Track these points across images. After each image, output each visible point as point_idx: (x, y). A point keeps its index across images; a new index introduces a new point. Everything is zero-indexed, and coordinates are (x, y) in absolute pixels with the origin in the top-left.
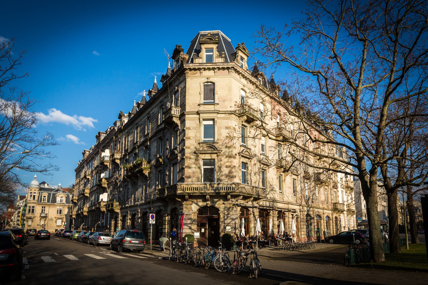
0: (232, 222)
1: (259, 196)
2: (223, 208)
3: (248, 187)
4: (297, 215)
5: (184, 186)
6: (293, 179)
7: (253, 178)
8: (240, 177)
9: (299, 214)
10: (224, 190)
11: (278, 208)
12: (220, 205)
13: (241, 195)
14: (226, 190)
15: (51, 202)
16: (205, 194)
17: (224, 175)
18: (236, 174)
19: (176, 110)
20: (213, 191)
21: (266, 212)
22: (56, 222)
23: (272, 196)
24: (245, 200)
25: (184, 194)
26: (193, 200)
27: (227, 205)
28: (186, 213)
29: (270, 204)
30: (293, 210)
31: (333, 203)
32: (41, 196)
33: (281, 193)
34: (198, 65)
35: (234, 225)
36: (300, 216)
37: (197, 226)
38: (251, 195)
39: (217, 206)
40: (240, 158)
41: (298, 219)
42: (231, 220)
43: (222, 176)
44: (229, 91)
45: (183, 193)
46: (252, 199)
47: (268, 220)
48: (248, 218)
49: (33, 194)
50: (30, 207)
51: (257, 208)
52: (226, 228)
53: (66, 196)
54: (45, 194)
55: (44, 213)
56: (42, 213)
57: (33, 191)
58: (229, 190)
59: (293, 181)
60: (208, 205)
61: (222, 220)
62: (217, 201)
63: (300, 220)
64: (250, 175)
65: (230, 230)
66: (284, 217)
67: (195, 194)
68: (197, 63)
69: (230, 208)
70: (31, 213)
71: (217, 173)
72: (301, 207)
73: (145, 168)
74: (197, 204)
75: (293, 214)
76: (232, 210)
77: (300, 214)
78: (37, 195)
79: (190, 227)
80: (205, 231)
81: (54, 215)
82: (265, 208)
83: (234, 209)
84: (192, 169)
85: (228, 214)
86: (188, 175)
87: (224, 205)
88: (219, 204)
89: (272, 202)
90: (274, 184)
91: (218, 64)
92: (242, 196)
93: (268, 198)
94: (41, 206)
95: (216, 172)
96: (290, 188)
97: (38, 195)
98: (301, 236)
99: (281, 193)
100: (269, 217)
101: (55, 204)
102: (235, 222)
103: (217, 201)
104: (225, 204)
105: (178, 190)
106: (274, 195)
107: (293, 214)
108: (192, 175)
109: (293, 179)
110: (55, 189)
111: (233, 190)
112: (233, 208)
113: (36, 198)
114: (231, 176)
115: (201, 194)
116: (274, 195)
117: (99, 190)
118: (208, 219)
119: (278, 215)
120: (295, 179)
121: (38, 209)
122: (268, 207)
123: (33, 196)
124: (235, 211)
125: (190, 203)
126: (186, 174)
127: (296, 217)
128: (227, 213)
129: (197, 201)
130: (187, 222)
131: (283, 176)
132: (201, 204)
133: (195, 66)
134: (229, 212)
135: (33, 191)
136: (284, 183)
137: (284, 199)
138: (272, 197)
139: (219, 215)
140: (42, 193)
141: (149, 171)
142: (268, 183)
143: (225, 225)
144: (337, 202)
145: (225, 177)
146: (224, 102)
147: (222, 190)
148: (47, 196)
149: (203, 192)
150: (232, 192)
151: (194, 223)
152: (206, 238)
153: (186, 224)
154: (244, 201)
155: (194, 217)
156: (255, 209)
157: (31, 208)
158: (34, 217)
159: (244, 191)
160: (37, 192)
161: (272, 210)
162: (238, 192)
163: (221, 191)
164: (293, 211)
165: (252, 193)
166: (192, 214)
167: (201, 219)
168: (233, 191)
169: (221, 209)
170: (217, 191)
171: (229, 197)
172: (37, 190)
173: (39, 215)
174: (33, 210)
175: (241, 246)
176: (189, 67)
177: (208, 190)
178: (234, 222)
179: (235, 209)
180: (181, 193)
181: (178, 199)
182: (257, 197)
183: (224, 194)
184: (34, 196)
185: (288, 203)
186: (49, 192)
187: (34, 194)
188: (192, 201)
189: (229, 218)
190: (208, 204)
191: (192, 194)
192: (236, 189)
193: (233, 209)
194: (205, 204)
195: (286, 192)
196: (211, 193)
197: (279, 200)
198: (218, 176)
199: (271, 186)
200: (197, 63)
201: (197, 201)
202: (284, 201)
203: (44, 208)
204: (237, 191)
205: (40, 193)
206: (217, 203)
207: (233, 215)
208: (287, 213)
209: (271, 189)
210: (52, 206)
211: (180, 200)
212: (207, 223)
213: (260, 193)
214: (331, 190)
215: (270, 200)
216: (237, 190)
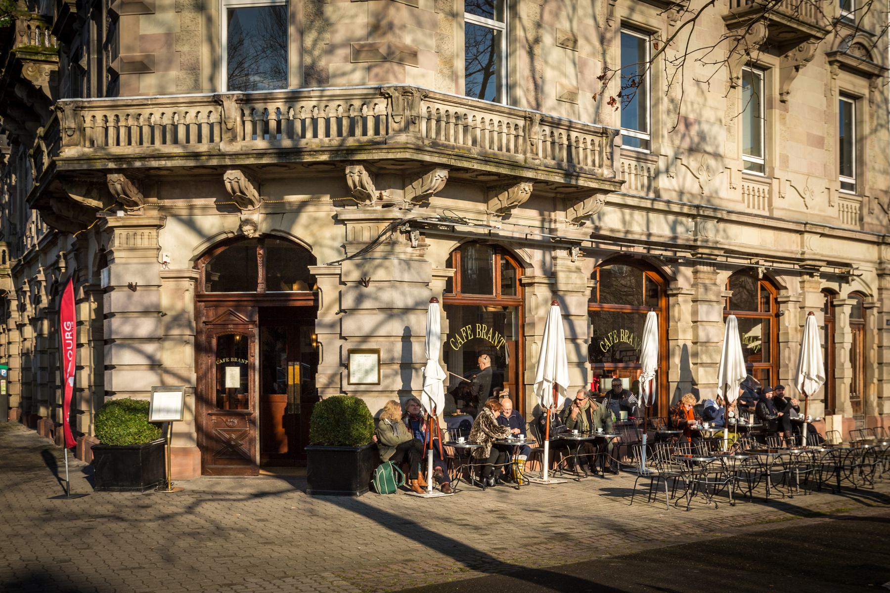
0: (383, 331)
1: (571, 172)
2: (338, 244)
3: (488, 117)
4: (856, 294)
6: (842, 93)
7: (549, 74)
8: (448, 62)
9: (875, 286)
10: (328, 134)
13: (433, 166)
14: (340, 133)
16: (214, 162)
17: (344, 45)
18: (420, 35)
20: (261, 144)
21: (654, 275)
23: (692, 186)
24: (486, 201)
25: (99, 165)
26: (167, 202)
27: (358, 226)
29: (680, 229)
30: (830, 263)
33: (760, 168)
35: (398, 347)
36: (881, 300)
37: (200, 349)
38: (514, 165)
39: (301, 232)
41: (864, 316)
42: (380, 317)
43: (331, 50)
45: (88, 159)
46: (524, 191)
48: (516, 308)
51: (576, 251)
52: (347, 366)
58: (352, 133)
59: (845, 110)
60: (248, 231)
61: (327, 314)
62: (303, 204)
63: (880, 320)
64: (531, 53)
65: (373, 378)
66: (778, 303)
67: (154, 164)
69: (375, 242)
71: (302, 33)
73: (34, 51)
74: (190, 224)
75: (834, 286)
76: (385, 258)
77: (880, 289)
79: (150, 357)
80: (244, 375)
82: (640, 249)
83: (398, 249)
84: (159, 16)
85: (363, 282)
86: (137, 55)
87: (340, 230)
88: (315, 220)
89: (693, 217)
90: (708, 114)
92: (443, 174)
93: (665, 196)
95: (292, 30)
96: (819, 142)
98: (880, 406)
99: (760, 168)
100: (672, 300)
102: (407, 330)
104: (343, 222)
105: (65, 140)
106: (703, 177)
107: (834, 286)
108: (159, 51)
109: (842, 93)
111: (377, 132)
112: (393, 244)
114: (383, 50)
115: (191, 163)
116: (703, 177)
118: (263, 312)
119: (730, 294)
120: (857, 98)
122: (665, 246)
124: (407, 263)
125: (149, 215)
126: (129, 48)
127: (854, 302)
128: (355, 275)
129: (191, 207)
130: (136, 327)
131: (776, 73)
134: (367, 267)
136: (776, 113)
137: (777, 202)
138: (696, 189)
139: (310, 282)
141: (55, 68)
142: (665, 105)
143: (348, 346)
145: (346, 59)
147: (315, 135)
149: (204, 147)
150: (374, 145)
151: (176, 332)
152: (253, 422)
153: (131, 342)
154: (482, 207)
156: (561, 254)
159: (457, 138)
161: (688, 263)
162: (405, 148)
163: (309, 141)
164: (830, 270)
165: (520, 157)
166: (163, 282)
167: (221, 311)
168: (378, 138)
170: (287, 143)
171: (357, 175)
175: (425, 469)
177: (234, 139)
178: (396, 328)
179: (405, 250)
180: (78, 159)
181: (87, 195)
182: (559, 179)
183: (324, 157)
185: (802, 229)
188: (161, 208)
189: (367, 304)
190: (247, 222)
191: (138, 164)
192: (393, 126)
193: (391, 252)
194: (231, 222)
196: (247, 155)
197: (731, 206)
198: (310, 52)
199: (688, 125)
201: (191, 207)
202: (776, 214)
204: (402, 138)
206: (304, 218)
207: (393, 284)
208: (791, 284)
209: (686, 144)
211: (94, 203)
212: (256, 331)
213: (586, 158)
215: (676, 208)
216: (400, 131)
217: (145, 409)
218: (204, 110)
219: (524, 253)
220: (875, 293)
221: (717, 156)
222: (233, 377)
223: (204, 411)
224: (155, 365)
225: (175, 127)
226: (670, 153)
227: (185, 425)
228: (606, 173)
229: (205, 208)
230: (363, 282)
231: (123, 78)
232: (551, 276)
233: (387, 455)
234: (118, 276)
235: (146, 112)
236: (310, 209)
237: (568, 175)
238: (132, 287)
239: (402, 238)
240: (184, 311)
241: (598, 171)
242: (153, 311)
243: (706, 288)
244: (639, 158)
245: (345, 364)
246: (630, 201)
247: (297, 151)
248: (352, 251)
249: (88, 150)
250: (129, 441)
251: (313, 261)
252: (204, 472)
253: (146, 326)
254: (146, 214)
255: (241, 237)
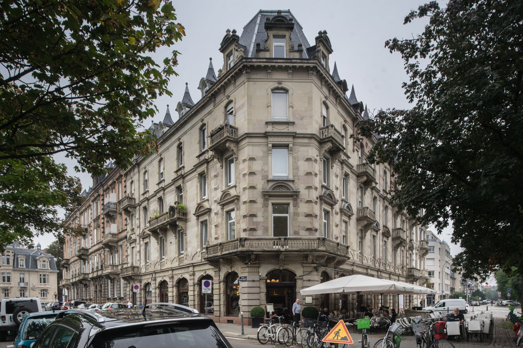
19: (232, 130)
28: (487, 281)
31: (409, 269)
34: (264, 60)
40: (321, 205)
44: (309, 103)
53: (50, 260)
55: (23, 282)
56: (21, 282)
68: (263, 59)
91: (293, 61)
117: (103, 250)
133: (260, 62)
137: (364, 262)
144: (412, 267)
146: (301, 119)
173: (17, 285)
176: (251, 64)
195: (366, 252)
200: (263, 59)
202: (364, 264)
214: (407, 251)
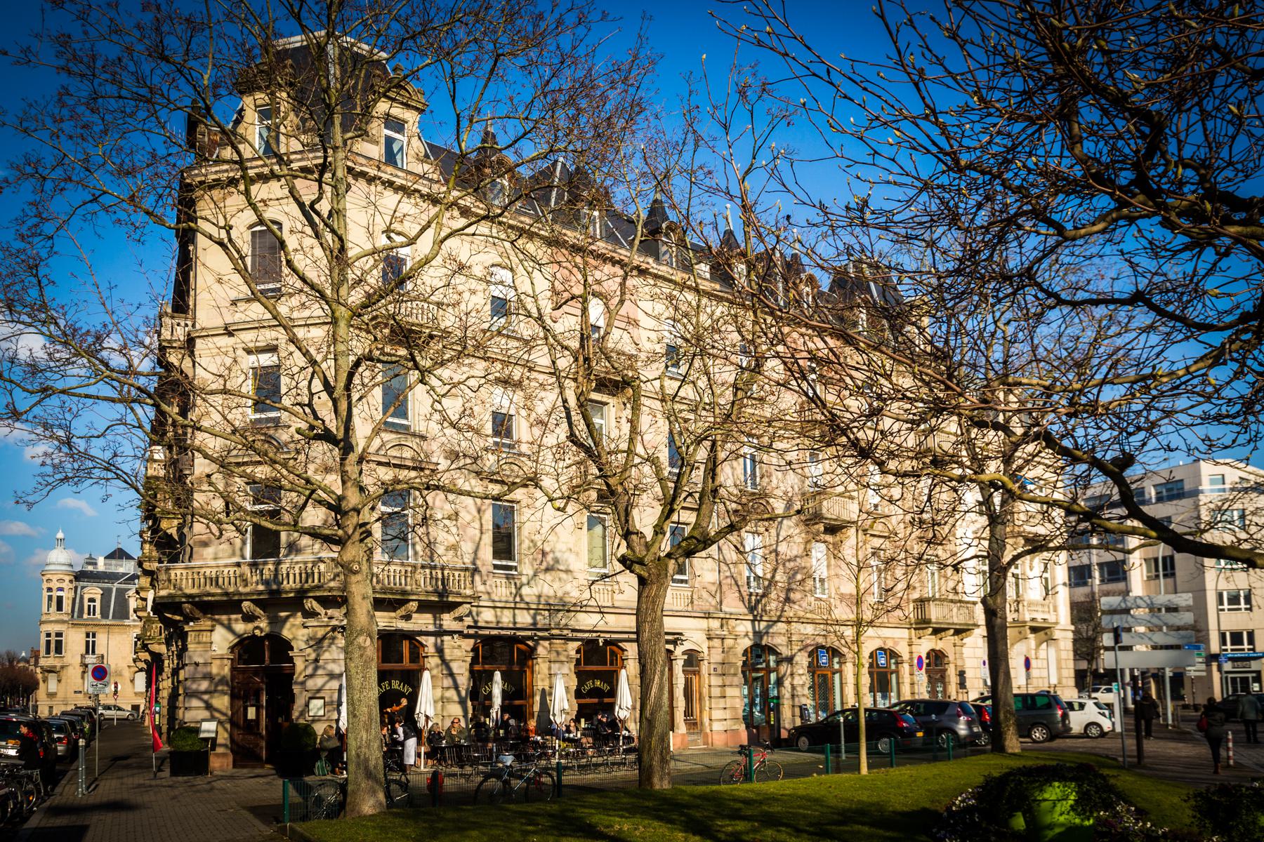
1: (443, 593)
5: (178, 572)
11: (574, 630)
12: (296, 631)
15: (114, 617)
16: (236, 598)
22: (132, 681)
23: (547, 590)
24: (394, 611)
25: (177, 600)
29: (539, 618)
31: (915, 601)
32: (82, 598)
37: (233, 697)
38: (404, 592)
39: (286, 633)
47: (532, 672)
49: (55, 594)
50: (48, 635)
54: (93, 591)
55: (93, 652)
56: (87, 652)
57: (55, 585)
58: (307, 581)
60: (257, 632)
62: (288, 617)
65: (321, 713)
69: (324, 638)
70: (52, 653)
72: (715, 624)
74: (229, 628)
78: (67, 596)
79: (206, 702)
81: (123, 658)
87: (306, 631)
90: (560, 546)
94: (83, 630)
97: (72, 594)
101: (127, 622)
103: (288, 617)
110: (125, 574)
112: (334, 638)
113: (67, 606)
121: (75, 641)
123: (55, 600)
128: (313, 656)
132: (240, 627)
135: (55, 585)
137: (617, 597)
138: (551, 593)
139: (291, 660)
140: (83, 588)
143: (310, 695)
148: (98, 598)
149: (231, 590)
150: (318, 587)
151: (220, 688)
152: (262, 737)
154: (393, 614)
155: (222, 669)
156: (446, 638)
157: (53, 639)
158: (62, 667)
160: (66, 585)
165: (408, 588)
169: (299, 644)
170: (274, 587)
172: (67, 578)
173: (78, 660)
174: (59, 645)
177: (246, 585)
181: (174, 614)
184: (60, 599)
186: (106, 585)
187: (60, 593)
189: (320, 672)
190: (257, 628)
203: (94, 636)
205: (76, 588)
206: (288, 625)
210: (116, 629)
211: (178, 618)
217: (197, 731)
218: (232, 570)
219: (422, 639)
220: (706, 651)
221: (567, 571)
222: (251, 713)
223: (236, 732)
224: (209, 707)
225: (217, 578)
226: (531, 573)
227: (223, 737)
228: (468, 592)
229: (236, 620)
230: (316, 660)
231: (195, 549)
232: (440, 651)
233: (324, 755)
234: (190, 657)
235: (202, 571)
236: (291, 620)
237: (440, 595)
238: (197, 664)
239: (339, 636)
240: (224, 677)
241: (462, 591)
242: (208, 677)
243: (558, 653)
244: (508, 577)
245: (307, 705)
246: (498, 604)
247: (279, 592)
248: (312, 643)
249: (172, 591)
250: (188, 748)
251: (292, 649)
252: (234, 766)
253: (204, 685)
254: (205, 623)
255: (254, 636)
